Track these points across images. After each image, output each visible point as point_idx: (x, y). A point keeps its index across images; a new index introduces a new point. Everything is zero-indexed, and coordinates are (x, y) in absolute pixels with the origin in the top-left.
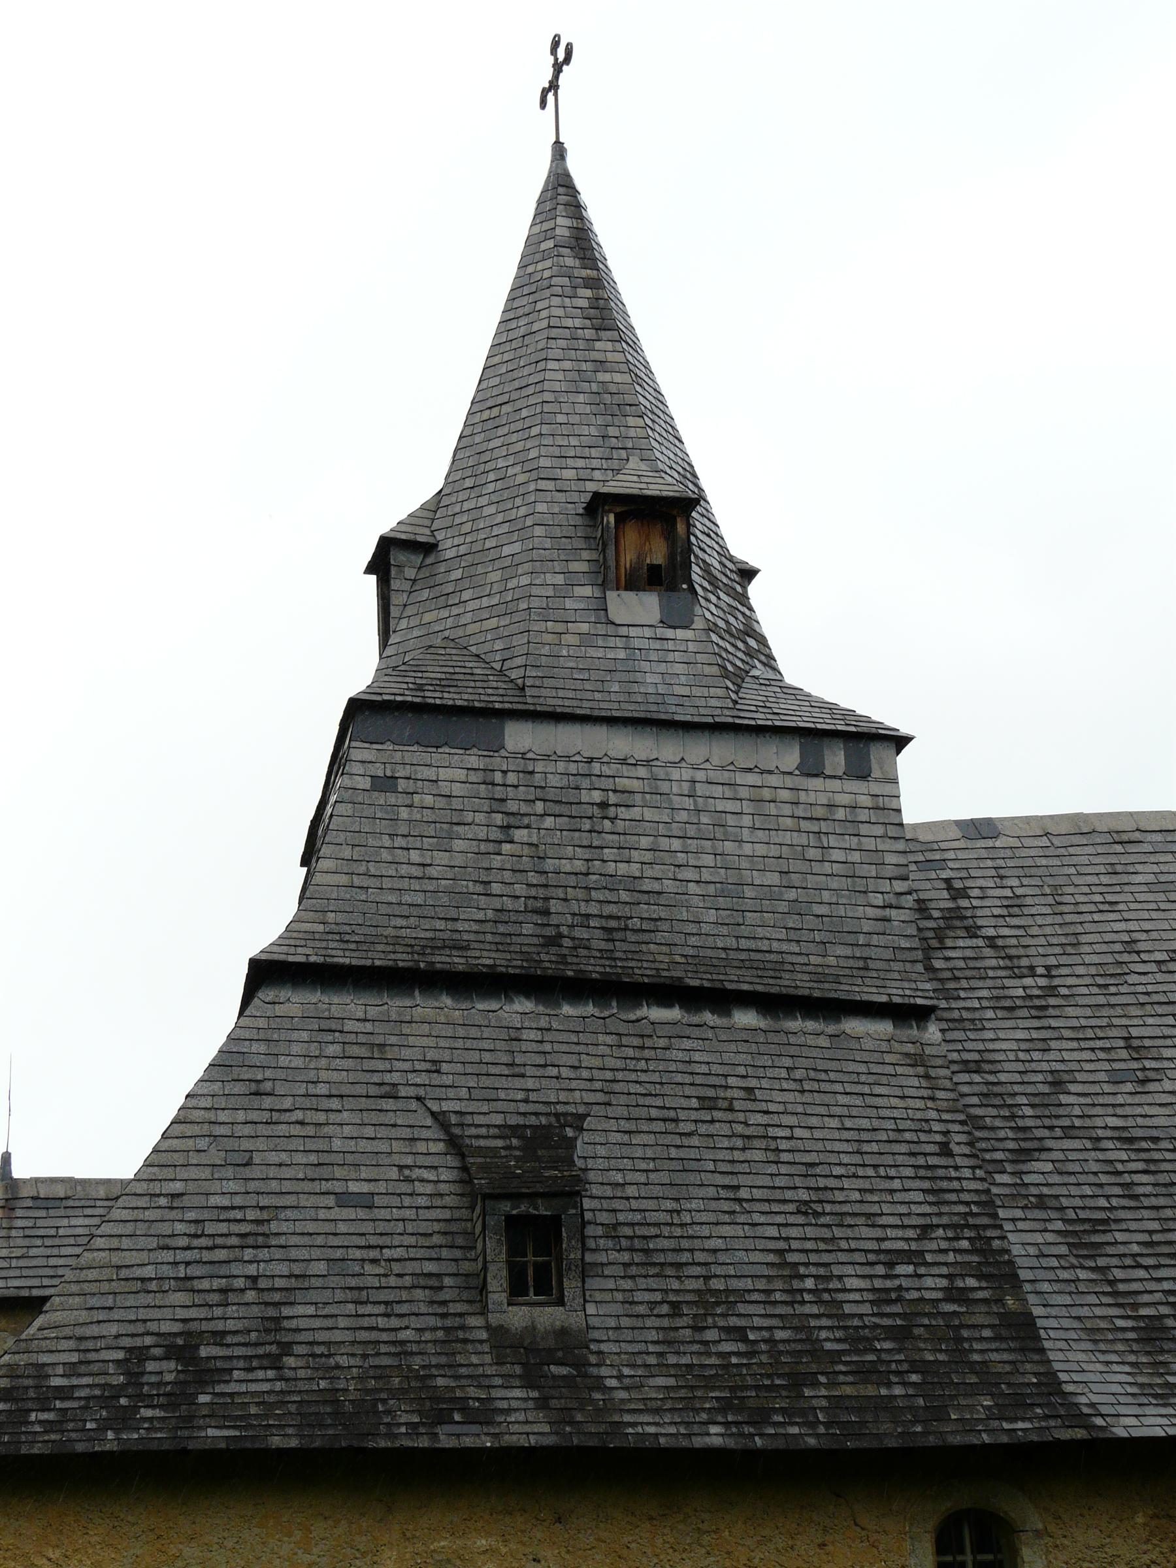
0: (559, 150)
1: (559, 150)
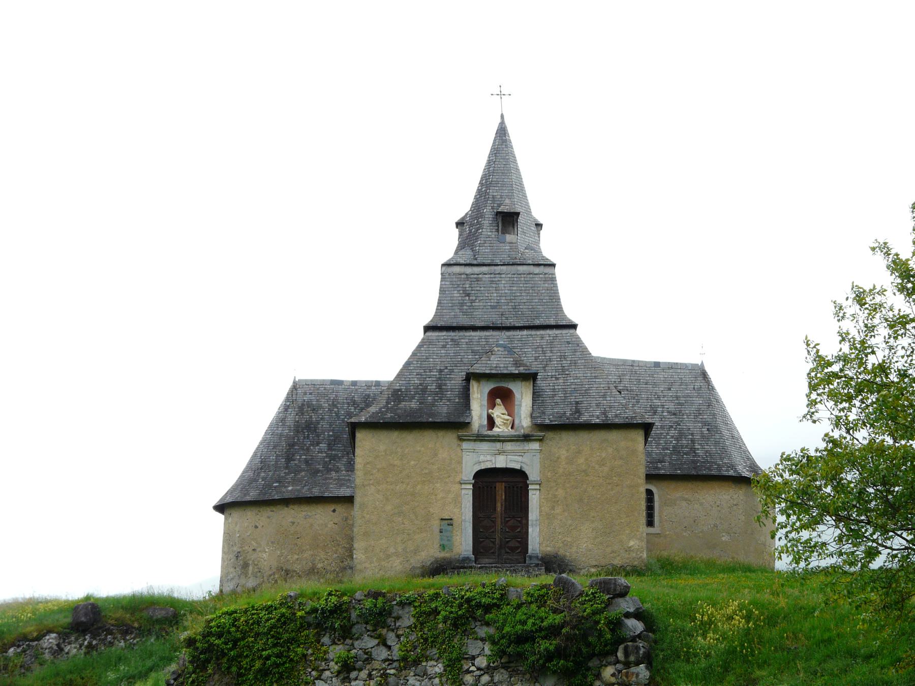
0: (502, 116)
1: (502, 116)
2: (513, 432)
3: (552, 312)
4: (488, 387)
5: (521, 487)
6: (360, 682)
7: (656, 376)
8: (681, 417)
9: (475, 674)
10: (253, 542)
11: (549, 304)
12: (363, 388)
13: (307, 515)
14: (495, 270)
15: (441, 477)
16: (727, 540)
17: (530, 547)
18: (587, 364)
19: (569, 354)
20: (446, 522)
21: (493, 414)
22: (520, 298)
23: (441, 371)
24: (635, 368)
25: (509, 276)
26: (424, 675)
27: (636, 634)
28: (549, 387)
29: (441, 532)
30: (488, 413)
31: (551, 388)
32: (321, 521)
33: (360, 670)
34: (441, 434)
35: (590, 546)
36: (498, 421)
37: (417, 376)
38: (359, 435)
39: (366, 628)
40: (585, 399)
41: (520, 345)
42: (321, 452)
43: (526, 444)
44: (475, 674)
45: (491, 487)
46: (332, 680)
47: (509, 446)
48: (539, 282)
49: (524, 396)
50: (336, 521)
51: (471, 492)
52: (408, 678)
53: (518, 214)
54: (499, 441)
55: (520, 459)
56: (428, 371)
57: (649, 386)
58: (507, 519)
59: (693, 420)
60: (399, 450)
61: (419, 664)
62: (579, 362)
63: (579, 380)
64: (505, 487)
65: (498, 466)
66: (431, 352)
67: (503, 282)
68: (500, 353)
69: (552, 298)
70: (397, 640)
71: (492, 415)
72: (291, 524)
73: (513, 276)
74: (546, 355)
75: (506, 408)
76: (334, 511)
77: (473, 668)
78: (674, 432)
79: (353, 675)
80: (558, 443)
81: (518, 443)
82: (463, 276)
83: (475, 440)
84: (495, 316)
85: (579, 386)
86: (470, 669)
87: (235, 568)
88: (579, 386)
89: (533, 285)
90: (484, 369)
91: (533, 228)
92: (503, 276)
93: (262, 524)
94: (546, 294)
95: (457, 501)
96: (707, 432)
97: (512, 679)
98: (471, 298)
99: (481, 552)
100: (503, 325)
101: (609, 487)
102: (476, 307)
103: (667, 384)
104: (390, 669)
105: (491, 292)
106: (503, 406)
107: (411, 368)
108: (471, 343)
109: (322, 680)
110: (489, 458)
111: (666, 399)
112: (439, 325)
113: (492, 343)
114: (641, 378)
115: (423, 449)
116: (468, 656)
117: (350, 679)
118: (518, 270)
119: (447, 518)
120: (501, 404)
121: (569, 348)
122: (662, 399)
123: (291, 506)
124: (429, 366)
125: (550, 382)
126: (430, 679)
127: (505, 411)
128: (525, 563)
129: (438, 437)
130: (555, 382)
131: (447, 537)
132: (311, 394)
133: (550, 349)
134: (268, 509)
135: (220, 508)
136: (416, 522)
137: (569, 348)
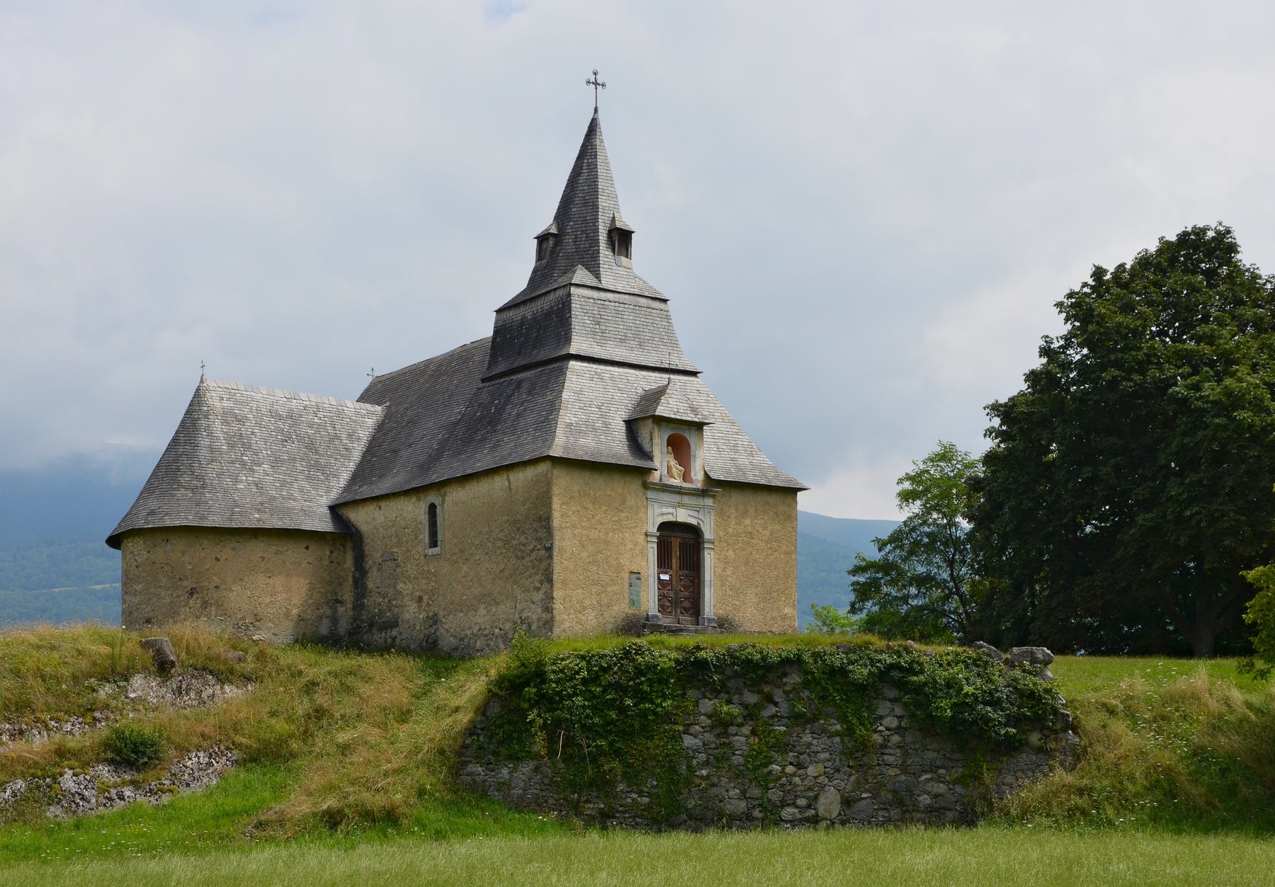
0: (596, 110)
1: (596, 110)
10: (214, 578)
14: (615, 297)
20: (635, 575)
25: (632, 307)
35: (754, 611)
39: (744, 683)
47: (686, 500)
50: (310, 560)
51: (655, 546)
52: (800, 735)
54: (679, 493)
60: (591, 492)
64: (680, 543)
76: (307, 548)
79: (733, 729)
81: (694, 498)
83: (658, 490)
92: (626, 306)
93: (225, 556)
95: (643, 553)
101: (770, 552)
104: (779, 726)
105: (618, 323)
109: (691, 734)
110: (671, 510)
131: (637, 592)
136: (610, 573)
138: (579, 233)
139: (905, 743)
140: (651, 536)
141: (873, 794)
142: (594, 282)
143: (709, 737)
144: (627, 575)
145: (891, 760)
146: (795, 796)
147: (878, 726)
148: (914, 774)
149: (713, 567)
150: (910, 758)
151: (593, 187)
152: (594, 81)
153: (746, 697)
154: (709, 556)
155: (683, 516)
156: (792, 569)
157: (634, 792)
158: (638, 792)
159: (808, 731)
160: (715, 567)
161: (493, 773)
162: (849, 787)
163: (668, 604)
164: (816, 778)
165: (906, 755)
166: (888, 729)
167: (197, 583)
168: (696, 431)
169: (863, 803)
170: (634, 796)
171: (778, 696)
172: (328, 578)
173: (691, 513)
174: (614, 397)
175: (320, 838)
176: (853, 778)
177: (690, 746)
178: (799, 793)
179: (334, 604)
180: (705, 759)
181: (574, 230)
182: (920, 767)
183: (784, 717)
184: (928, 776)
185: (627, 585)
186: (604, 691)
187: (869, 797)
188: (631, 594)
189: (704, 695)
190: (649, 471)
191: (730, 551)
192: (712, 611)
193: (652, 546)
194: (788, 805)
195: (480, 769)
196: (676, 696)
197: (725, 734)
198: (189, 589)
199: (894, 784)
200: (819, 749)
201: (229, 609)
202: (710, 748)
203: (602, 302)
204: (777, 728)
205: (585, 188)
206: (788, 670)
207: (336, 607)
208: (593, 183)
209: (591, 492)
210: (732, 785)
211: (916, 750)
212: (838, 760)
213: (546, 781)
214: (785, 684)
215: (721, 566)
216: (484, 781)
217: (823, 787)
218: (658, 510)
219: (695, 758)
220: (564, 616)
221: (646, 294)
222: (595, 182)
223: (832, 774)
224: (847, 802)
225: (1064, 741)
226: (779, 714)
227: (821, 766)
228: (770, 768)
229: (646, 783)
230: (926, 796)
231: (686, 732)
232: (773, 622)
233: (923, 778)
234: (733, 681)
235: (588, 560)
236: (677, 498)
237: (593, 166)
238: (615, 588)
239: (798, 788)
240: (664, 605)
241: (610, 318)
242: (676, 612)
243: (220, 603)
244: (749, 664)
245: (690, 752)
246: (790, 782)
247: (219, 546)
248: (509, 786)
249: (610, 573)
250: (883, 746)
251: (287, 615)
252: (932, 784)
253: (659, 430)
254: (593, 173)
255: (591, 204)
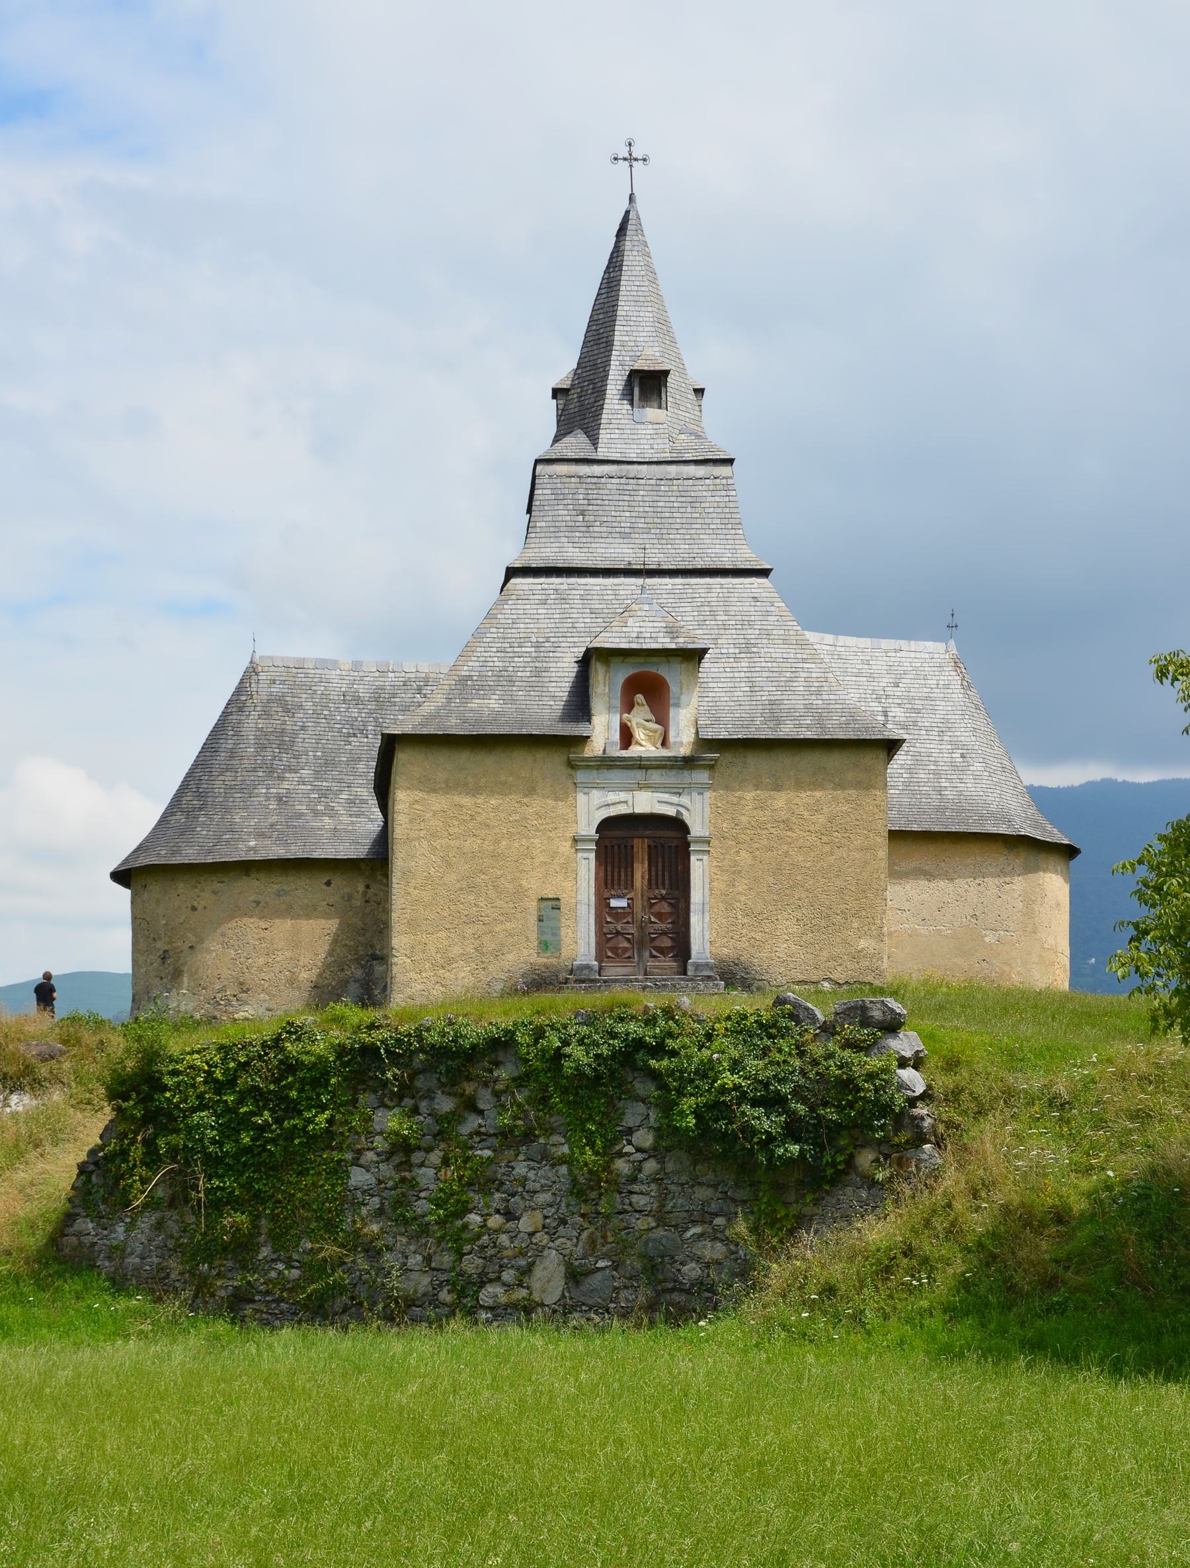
0: (631, 198)
1: (631, 198)
2: (665, 753)
3: (727, 547)
4: (622, 674)
5: (677, 847)
6: (427, 1170)
7: (874, 662)
8: (916, 732)
9: (631, 1158)
10: (189, 935)
11: (720, 531)
12: (373, 675)
13: (283, 890)
14: (628, 471)
15: (542, 828)
16: (992, 941)
17: (694, 953)
18: (787, 637)
19: (757, 618)
20: (550, 903)
21: (630, 721)
22: (670, 521)
23: (538, 645)
24: (838, 649)
26: (542, 1159)
27: (917, 1094)
28: (724, 675)
29: (540, 920)
30: (621, 719)
31: (728, 675)
32: (306, 901)
33: (429, 1150)
34: (541, 755)
36: (639, 734)
37: (499, 654)
38: (402, 758)
40: (786, 697)
41: (671, 601)
42: (304, 783)
43: (686, 773)
44: (631, 1158)
45: (626, 846)
46: (378, 1167)
47: (656, 777)
48: (705, 494)
49: (684, 690)
50: (331, 901)
51: (592, 856)
52: (513, 1164)
53: (666, 373)
54: (640, 767)
55: (675, 799)
56: (516, 645)
57: (861, 679)
58: (653, 901)
59: (937, 738)
60: (470, 779)
61: (534, 1142)
62: (775, 632)
63: (775, 664)
64: (649, 846)
65: (639, 809)
66: (522, 612)
67: (642, 493)
68: (644, 613)
69: (726, 521)
70: (496, 1099)
71: (629, 724)
72: (254, 905)
73: (658, 482)
74: (717, 618)
75: (652, 711)
76: (328, 883)
77: (629, 1149)
78: (905, 757)
79: (417, 1157)
80: (740, 773)
81: (674, 772)
82: (573, 480)
83: (598, 768)
84: (628, 551)
85: (775, 674)
86: (624, 1151)
87: (161, 978)
88: (775, 674)
89: (694, 499)
90: (617, 640)
91: (690, 396)
92: (641, 482)
93: (203, 903)
94: (715, 515)
95: (568, 869)
96: (961, 760)
97: (698, 1168)
98: (587, 518)
99: (609, 957)
100: (647, 567)
101: (827, 848)
102: (596, 535)
103: (893, 676)
104: (481, 1149)
106: (647, 707)
107: (488, 640)
108: (588, 597)
109: (361, 1166)
110: (623, 796)
111: (890, 701)
112: (533, 566)
113: (625, 597)
114: (848, 666)
115: (511, 779)
116: (621, 1128)
117: (411, 1165)
118: (668, 473)
119: (550, 896)
120: (645, 703)
121: (757, 609)
122: (883, 701)
123: (254, 875)
124: (517, 636)
125: (726, 665)
126: (553, 1166)
127: (650, 716)
128: (685, 974)
129: (535, 761)
130: (735, 665)
132: (283, 682)
133: (723, 608)
134: (214, 878)
135: (122, 876)
136: (499, 903)
137: (757, 609)
138: (586, 384)
139: (666, 1174)
140: (583, 841)
141: (614, 1262)
142: (587, 452)
143: (386, 1170)
144: (535, 903)
145: (642, 1203)
146: (501, 1266)
147: (624, 1146)
148: (676, 1226)
149: (707, 880)
150: (672, 1199)
151: (610, 314)
152: (627, 155)
153: (438, 1104)
154: (700, 863)
155: (646, 802)
156: (875, 876)
157: (281, 1261)
158: (286, 1260)
159: (521, 1157)
160: (711, 881)
161: (105, 1232)
162: (579, 1250)
163: (626, 944)
164: (531, 1234)
165: (664, 1196)
166: (639, 1150)
167: (170, 943)
168: (681, 663)
169: (599, 1276)
170: (281, 1266)
171: (485, 1100)
172: (360, 924)
173: (666, 797)
174: (576, 625)
175: (638, 1326)
176: (585, 1235)
177: (360, 1184)
178: (506, 1261)
179: (368, 961)
180: (377, 1206)
181: (581, 380)
182: (685, 1215)
183: (490, 1135)
184: (697, 1230)
185: (533, 920)
186: (241, 1102)
187: (607, 1267)
188: (541, 932)
189: (383, 1102)
190: (584, 740)
191: (743, 853)
192: (707, 951)
193: (586, 855)
194: (491, 1281)
195: (90, 1225)
196: (341, 1105)
197: (407, 1165)
198: (161, 952)
199: (646, 1243)
200: (537, 1186)
201: (205, 977)
202: (386, 1188)
203: (595, 480)
204: (479, 1152)
205: (601, 316)
206: (501, 1056)
207: (371, 965)
208: (611, 309)
209: (470, 779)
210: (412, 1248)
211: (682, 1185)
212: (563, 1205)
213: (171, 1244)
214: (496, 1081)
215: (725, 878)
216: (94, 1244)
217: (540, 1250)
218: (597, 797)
219: (365, 1205)
220: (412, 975)
221: (688, 457)
222: (614, 306)
223: (555, 1228)
224: (575, 1276)
225: (914, 1163)
226: (483, 1130)
227: (538, 1215)
228: (466, 1219)
229: (297, 1246)
230: (693, 1265)
231: (356, 1162)
232: (832, 964)
233: (689, 1234)
234: (421, 1077)
235: (458, 885)
236: (639, 775)
237: (615, 283)
238: (509, 926)
239: (505, 1253)
240: (618, 948)
241: (606, 502)
242: (640, 956)
243: (193, 970)
244: (440, 1053)
245: (359, 1194)
246: (494, 1243)
247: (197, 890)
248: (124, 1251)
249: (499, 903)
250: (633, 1179)
251: (292, 981)
252: (704, 1243)
253: (607, 671)
254: (613, 294)
255: (604, 340)
